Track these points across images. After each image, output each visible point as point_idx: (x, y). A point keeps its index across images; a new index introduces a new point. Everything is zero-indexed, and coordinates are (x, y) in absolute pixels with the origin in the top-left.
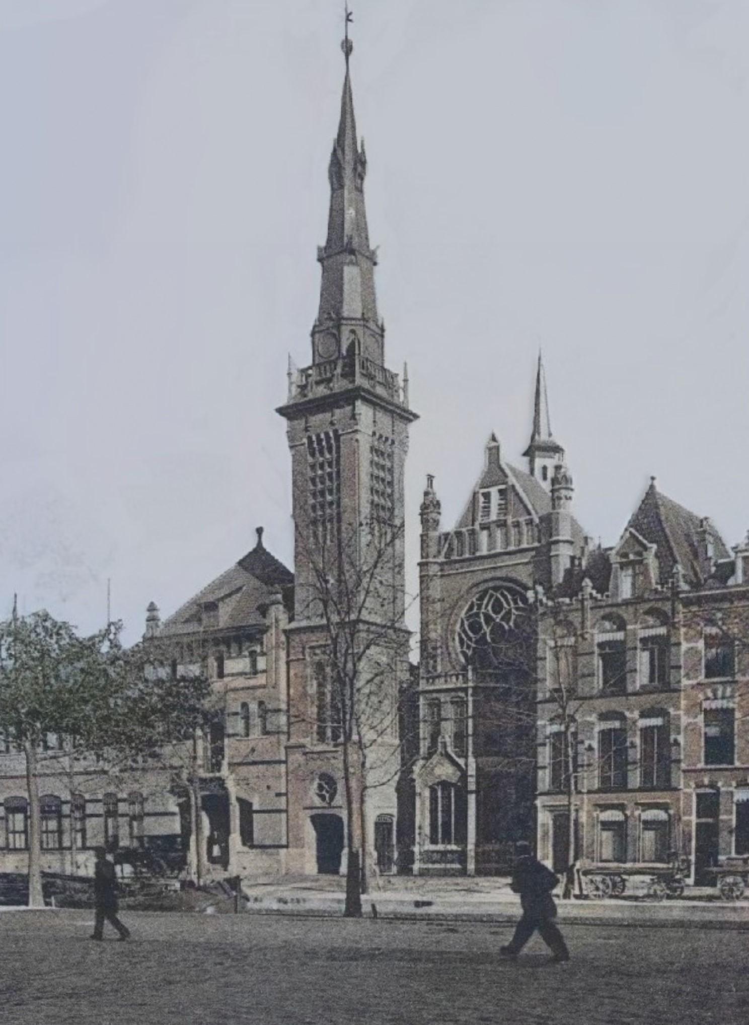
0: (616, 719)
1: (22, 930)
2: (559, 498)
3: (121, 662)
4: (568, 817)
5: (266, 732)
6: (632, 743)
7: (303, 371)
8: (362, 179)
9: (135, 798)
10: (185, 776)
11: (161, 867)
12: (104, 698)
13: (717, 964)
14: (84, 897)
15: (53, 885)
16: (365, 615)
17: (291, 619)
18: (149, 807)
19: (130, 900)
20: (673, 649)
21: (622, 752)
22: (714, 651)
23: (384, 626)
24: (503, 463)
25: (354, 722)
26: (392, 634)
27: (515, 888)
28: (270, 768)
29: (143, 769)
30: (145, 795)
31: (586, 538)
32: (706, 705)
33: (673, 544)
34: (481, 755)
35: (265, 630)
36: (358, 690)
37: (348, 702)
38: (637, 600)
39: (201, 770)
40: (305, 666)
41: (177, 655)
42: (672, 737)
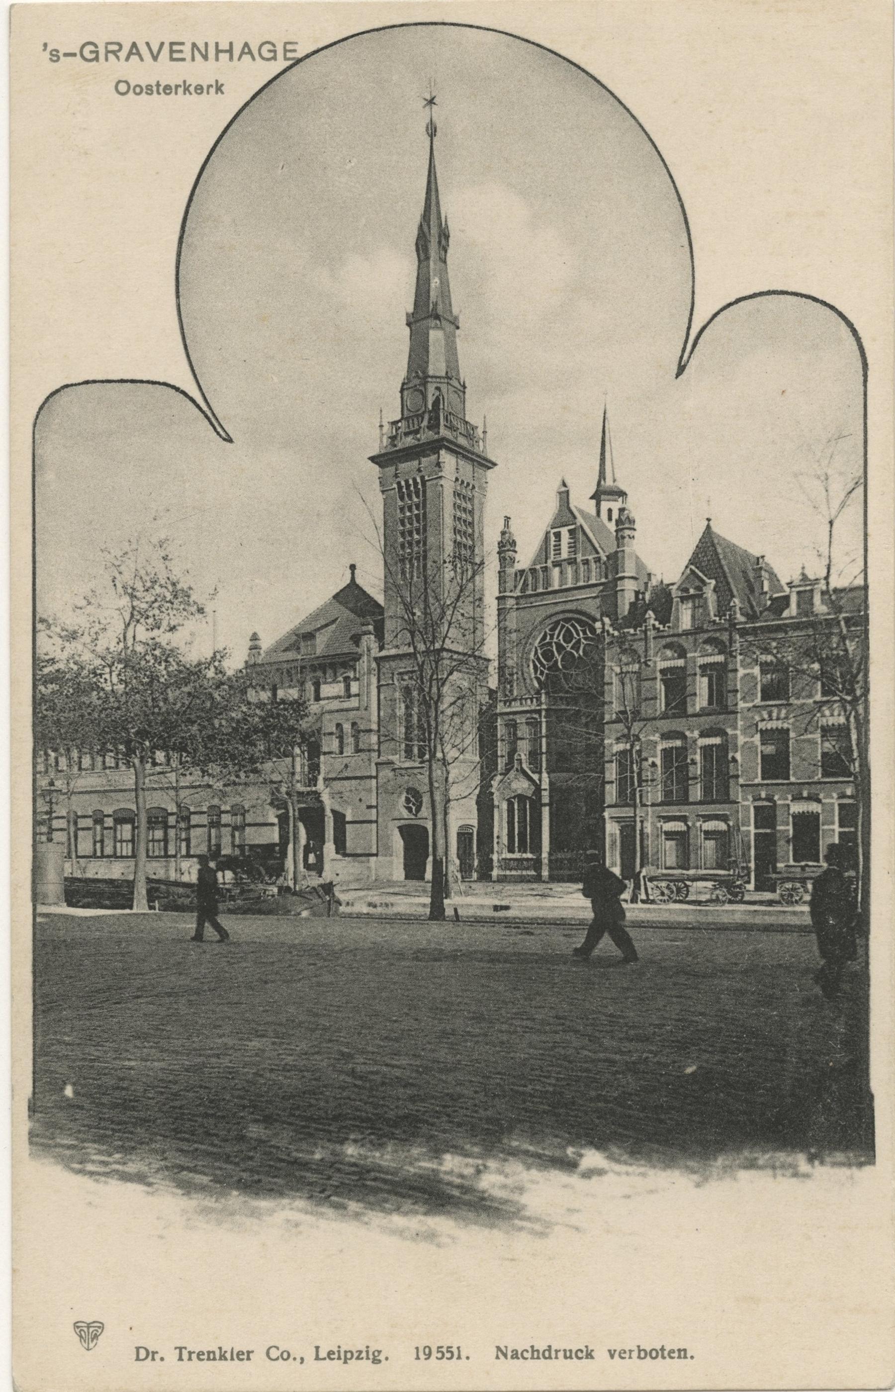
0: (677, 738)
1: (125, 932)
2: (623, 537)
3: (226, 687)
4: (634, 828)
5: (358, 750)
6: (692, 760)
7: (394, 423)
8: (446, 252)
9: (238, 810)
10: (284, 789)
11: (260, 874)
12: (209, 720)
13: (780, 965)
14: (187, 901)
15: (157, 890)
16: (448, 644)
17: (381, 648)
18: (249, 819)
19: (231, 904)
20: (730, 675)
21: (683, 768)
22: (769, 676)
23: (465, 654)
24: (572, 506)
25: (438, 741)
26: (472, 661)
27: (586, 893)
28: (362, 782)
29: (246, 784)
30: (246, 808)
31: (649, 575)
32: (761, 726)
33: (730, 580)
34: (554, 772)
35: (357, 658)
36: (442, 712)
37: (433, 723)
38: (697, 630)
39: (299, 785)
40: (395, 690)
41: (277, 680)
42: (730, 755)
